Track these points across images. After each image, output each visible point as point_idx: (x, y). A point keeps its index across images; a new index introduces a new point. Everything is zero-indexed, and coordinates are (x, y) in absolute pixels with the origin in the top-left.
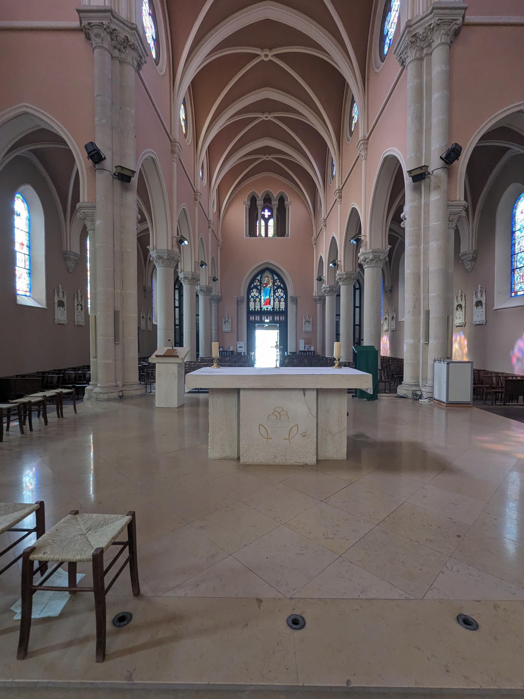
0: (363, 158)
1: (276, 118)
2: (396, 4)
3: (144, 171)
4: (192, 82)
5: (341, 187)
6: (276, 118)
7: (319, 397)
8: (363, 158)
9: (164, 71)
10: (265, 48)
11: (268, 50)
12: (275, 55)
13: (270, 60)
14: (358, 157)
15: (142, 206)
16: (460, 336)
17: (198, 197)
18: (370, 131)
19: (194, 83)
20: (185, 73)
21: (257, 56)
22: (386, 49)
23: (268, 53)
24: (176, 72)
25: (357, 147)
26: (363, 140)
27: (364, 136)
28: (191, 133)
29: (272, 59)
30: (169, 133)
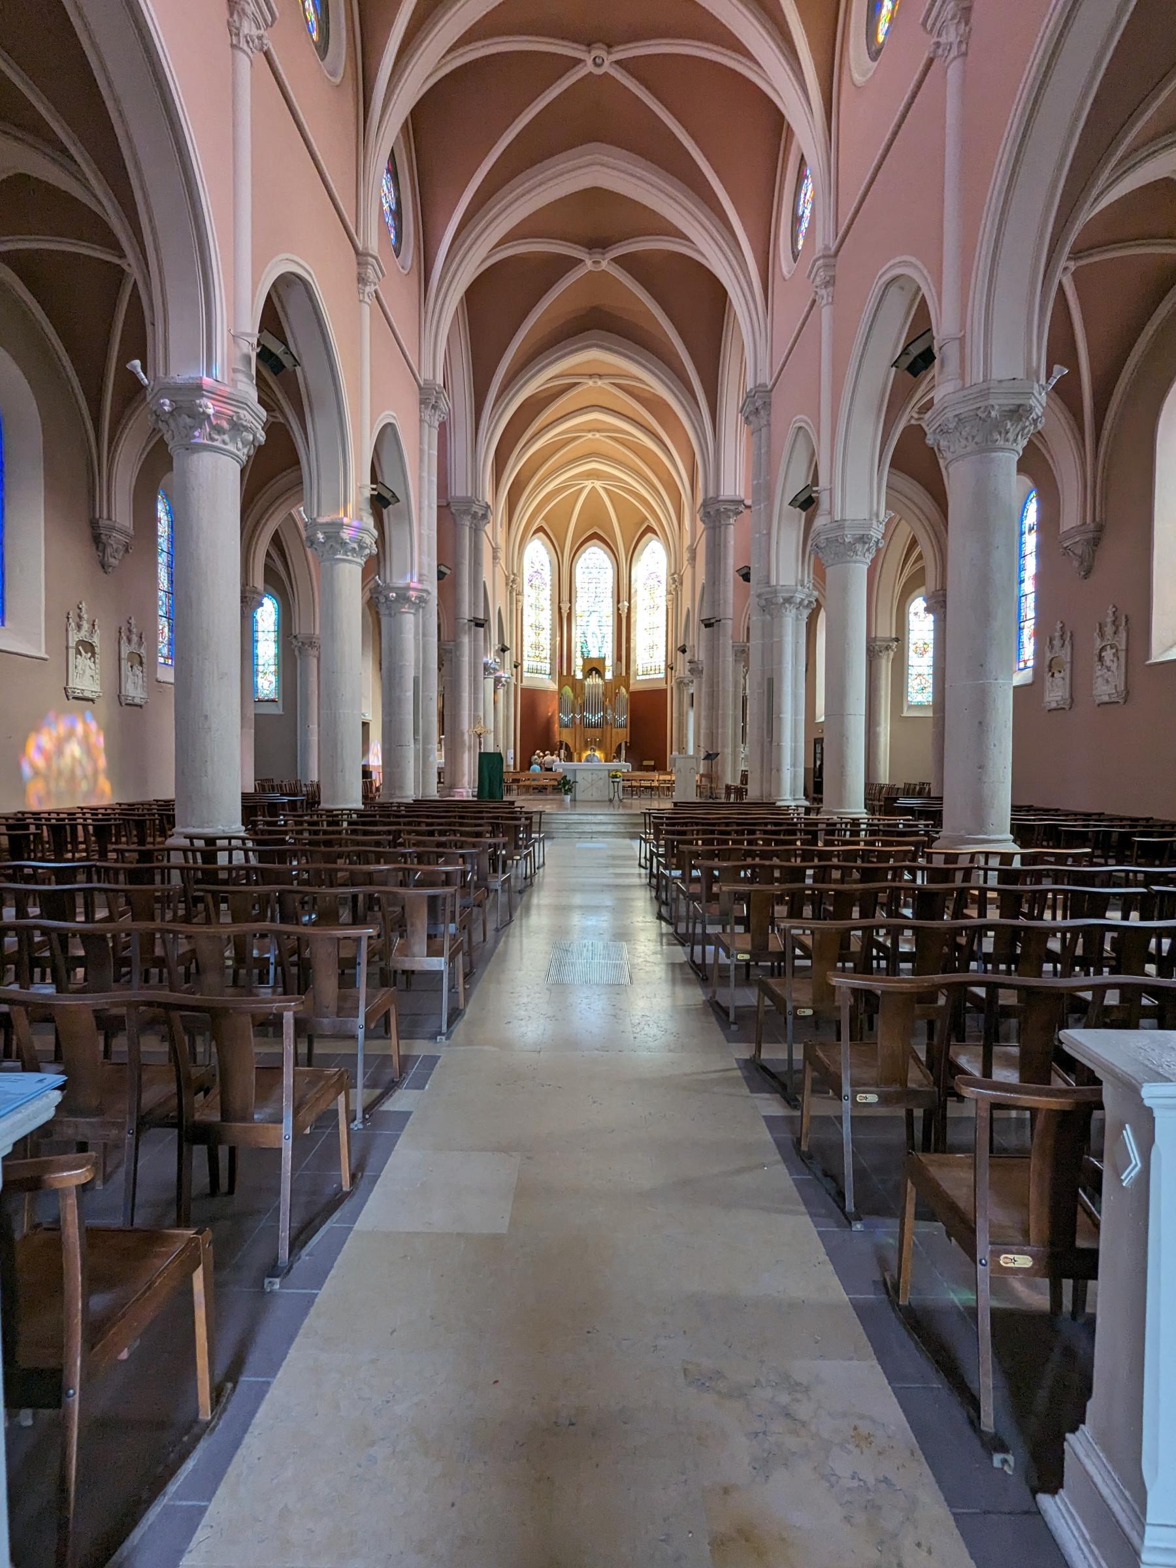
0: (824, 302)
1: (605, 489)
2: (887, 5)
3: (279, 297)
4: (413, 113)
5: (833, 249)
6: (605, 489)
7: (316, 419)
8: (824, 302)
9: (341, 71)
10: (595, 42)
11: (604, 47)
12: (618, 62)
13: (606, 74)
14: (814, 301)
15: (110, 210)
16: (85, 723)
17: (370, 271)
18: (840, 235)
19: (416, 113)
20: (395, 86)
21: (577, 62)
22: (801, 243)
23: (603, 54)
24: (373, 88)
25: (809, 276)
26: (824, 257)
27: (827, 248)
28: (412, 244)
29: (612, 72)
30: (353, 231)
